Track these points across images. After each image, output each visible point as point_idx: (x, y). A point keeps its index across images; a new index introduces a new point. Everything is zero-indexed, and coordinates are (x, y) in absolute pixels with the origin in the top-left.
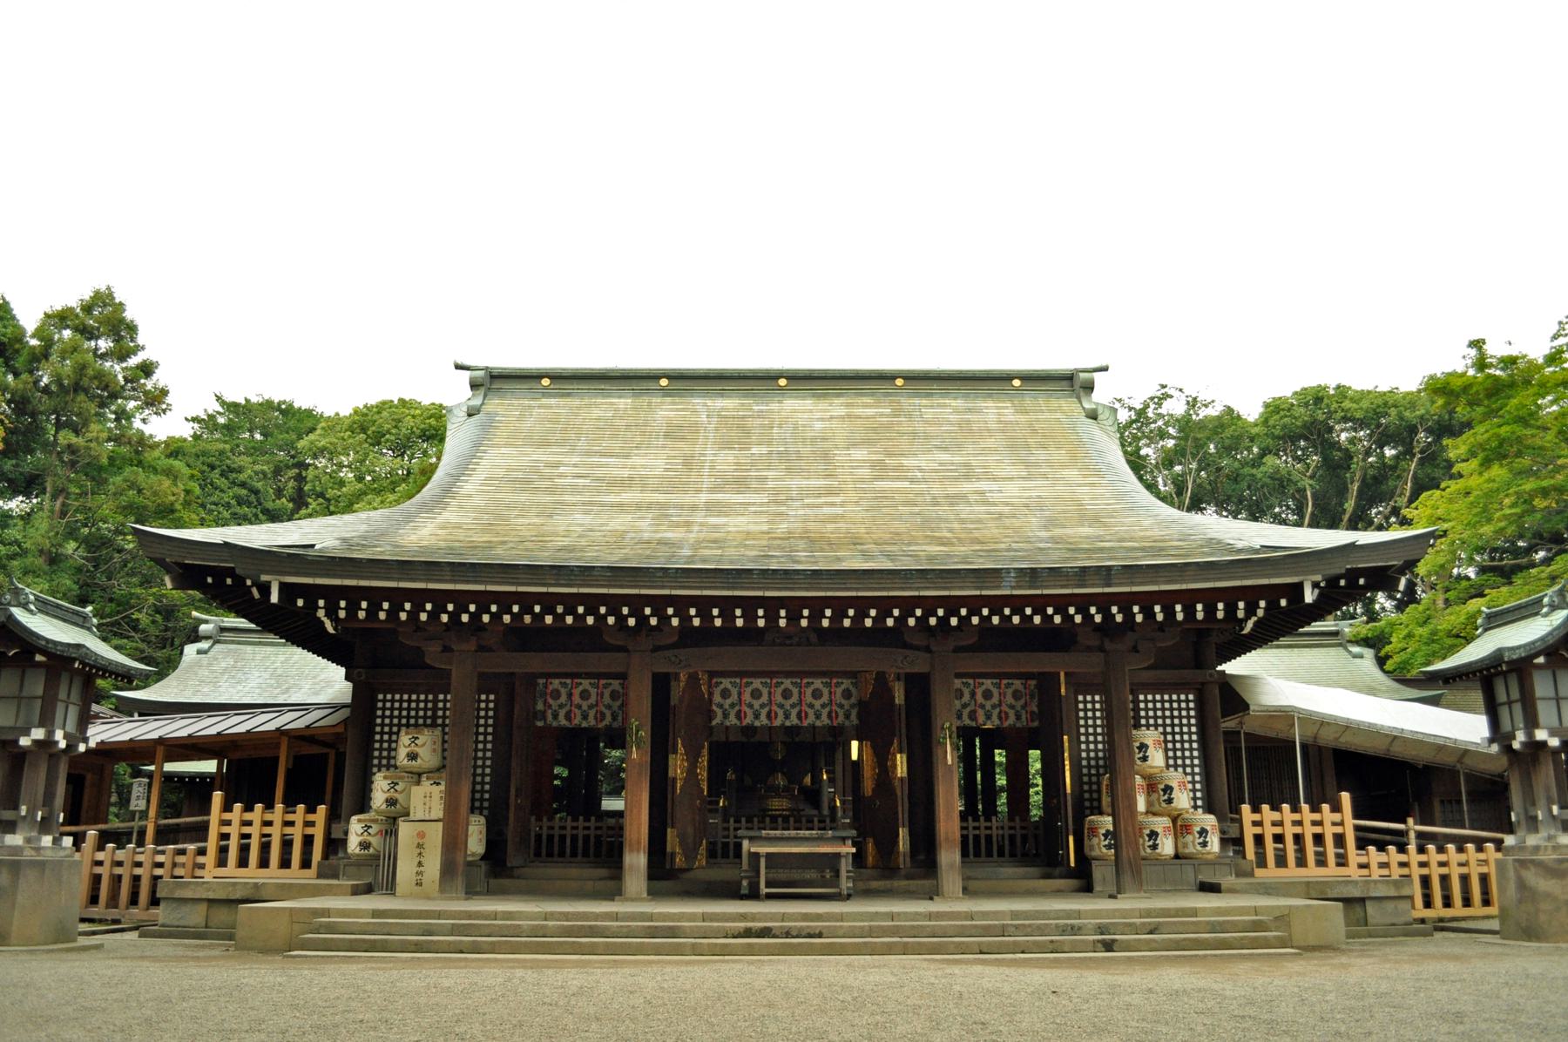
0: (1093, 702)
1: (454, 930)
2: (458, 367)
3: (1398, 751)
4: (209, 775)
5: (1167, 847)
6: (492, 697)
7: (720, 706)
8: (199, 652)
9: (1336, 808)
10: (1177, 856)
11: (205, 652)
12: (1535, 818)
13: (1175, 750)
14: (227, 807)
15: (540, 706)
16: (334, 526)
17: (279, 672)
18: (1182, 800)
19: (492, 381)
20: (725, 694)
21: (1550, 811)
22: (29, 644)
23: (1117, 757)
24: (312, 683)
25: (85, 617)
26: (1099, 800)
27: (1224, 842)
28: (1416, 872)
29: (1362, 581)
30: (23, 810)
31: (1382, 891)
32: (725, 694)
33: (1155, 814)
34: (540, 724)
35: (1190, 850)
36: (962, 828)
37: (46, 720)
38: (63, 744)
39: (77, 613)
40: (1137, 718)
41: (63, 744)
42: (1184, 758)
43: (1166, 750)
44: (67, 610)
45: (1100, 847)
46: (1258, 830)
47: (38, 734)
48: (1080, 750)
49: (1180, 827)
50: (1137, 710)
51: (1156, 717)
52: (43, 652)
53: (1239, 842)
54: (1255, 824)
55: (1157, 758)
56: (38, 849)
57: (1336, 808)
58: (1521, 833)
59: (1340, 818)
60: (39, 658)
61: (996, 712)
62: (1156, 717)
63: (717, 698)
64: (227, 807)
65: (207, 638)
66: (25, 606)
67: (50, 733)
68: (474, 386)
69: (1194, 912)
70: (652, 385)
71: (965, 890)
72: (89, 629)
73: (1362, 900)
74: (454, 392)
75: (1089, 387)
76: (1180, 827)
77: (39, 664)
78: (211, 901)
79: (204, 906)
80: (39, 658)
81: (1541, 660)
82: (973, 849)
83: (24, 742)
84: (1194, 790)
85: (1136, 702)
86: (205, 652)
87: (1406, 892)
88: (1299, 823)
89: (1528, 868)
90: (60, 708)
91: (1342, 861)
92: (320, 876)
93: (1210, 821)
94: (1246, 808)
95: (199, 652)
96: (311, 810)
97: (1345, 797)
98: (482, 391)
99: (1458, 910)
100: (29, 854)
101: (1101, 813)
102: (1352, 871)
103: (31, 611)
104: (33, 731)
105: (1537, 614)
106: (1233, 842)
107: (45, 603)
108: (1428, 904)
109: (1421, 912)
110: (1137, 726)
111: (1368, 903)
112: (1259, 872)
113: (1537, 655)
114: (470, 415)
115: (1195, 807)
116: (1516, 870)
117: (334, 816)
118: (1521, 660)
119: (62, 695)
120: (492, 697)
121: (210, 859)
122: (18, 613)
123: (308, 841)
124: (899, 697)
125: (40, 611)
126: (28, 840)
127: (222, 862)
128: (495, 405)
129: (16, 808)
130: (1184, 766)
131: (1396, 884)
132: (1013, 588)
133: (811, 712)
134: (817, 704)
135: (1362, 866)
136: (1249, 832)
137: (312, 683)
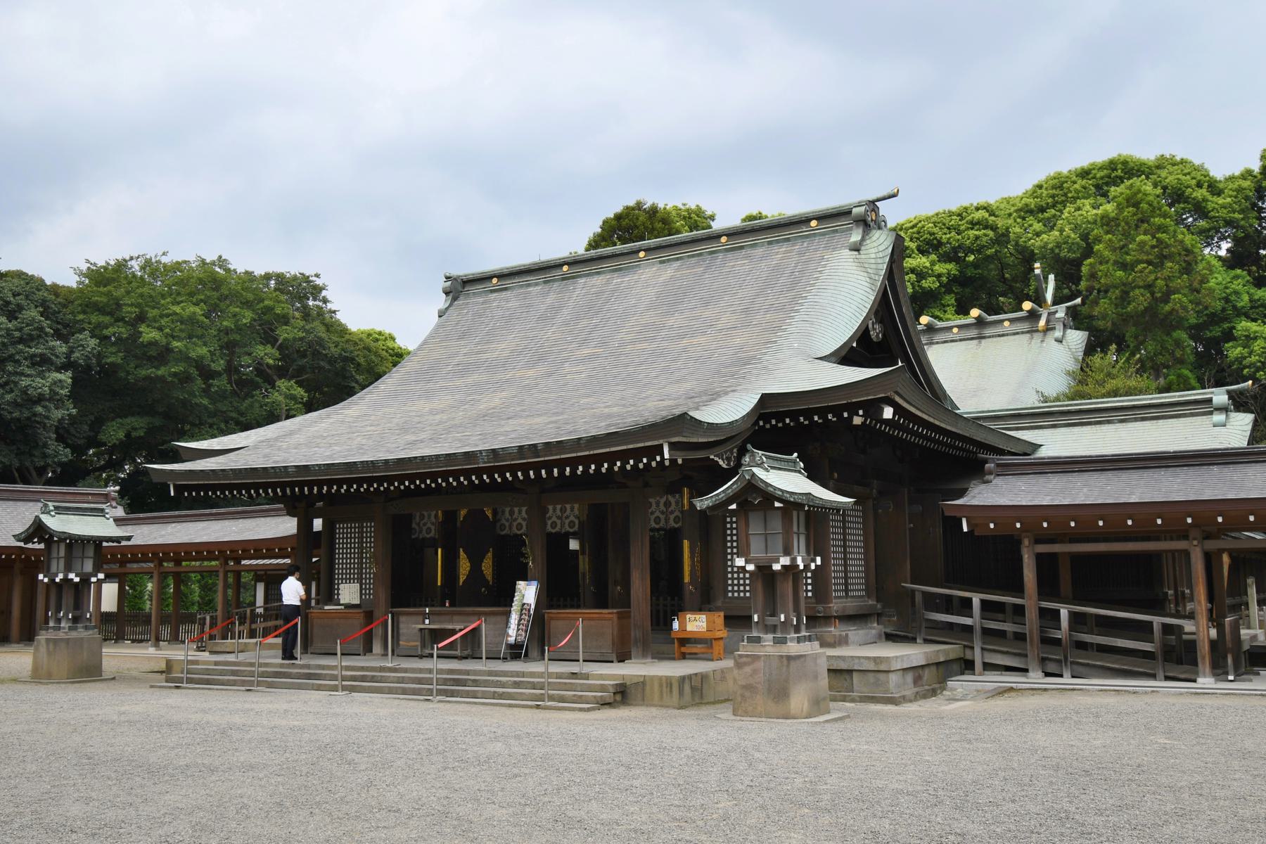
37: (787, 551)
39: (788, 461)
47: (785, 561)
60: (777, 504)
67: (794, 560)
70: (557, 273)
73: (850, 672)
80: (777, 504)
81: (734, 507)
83: (777, 567)
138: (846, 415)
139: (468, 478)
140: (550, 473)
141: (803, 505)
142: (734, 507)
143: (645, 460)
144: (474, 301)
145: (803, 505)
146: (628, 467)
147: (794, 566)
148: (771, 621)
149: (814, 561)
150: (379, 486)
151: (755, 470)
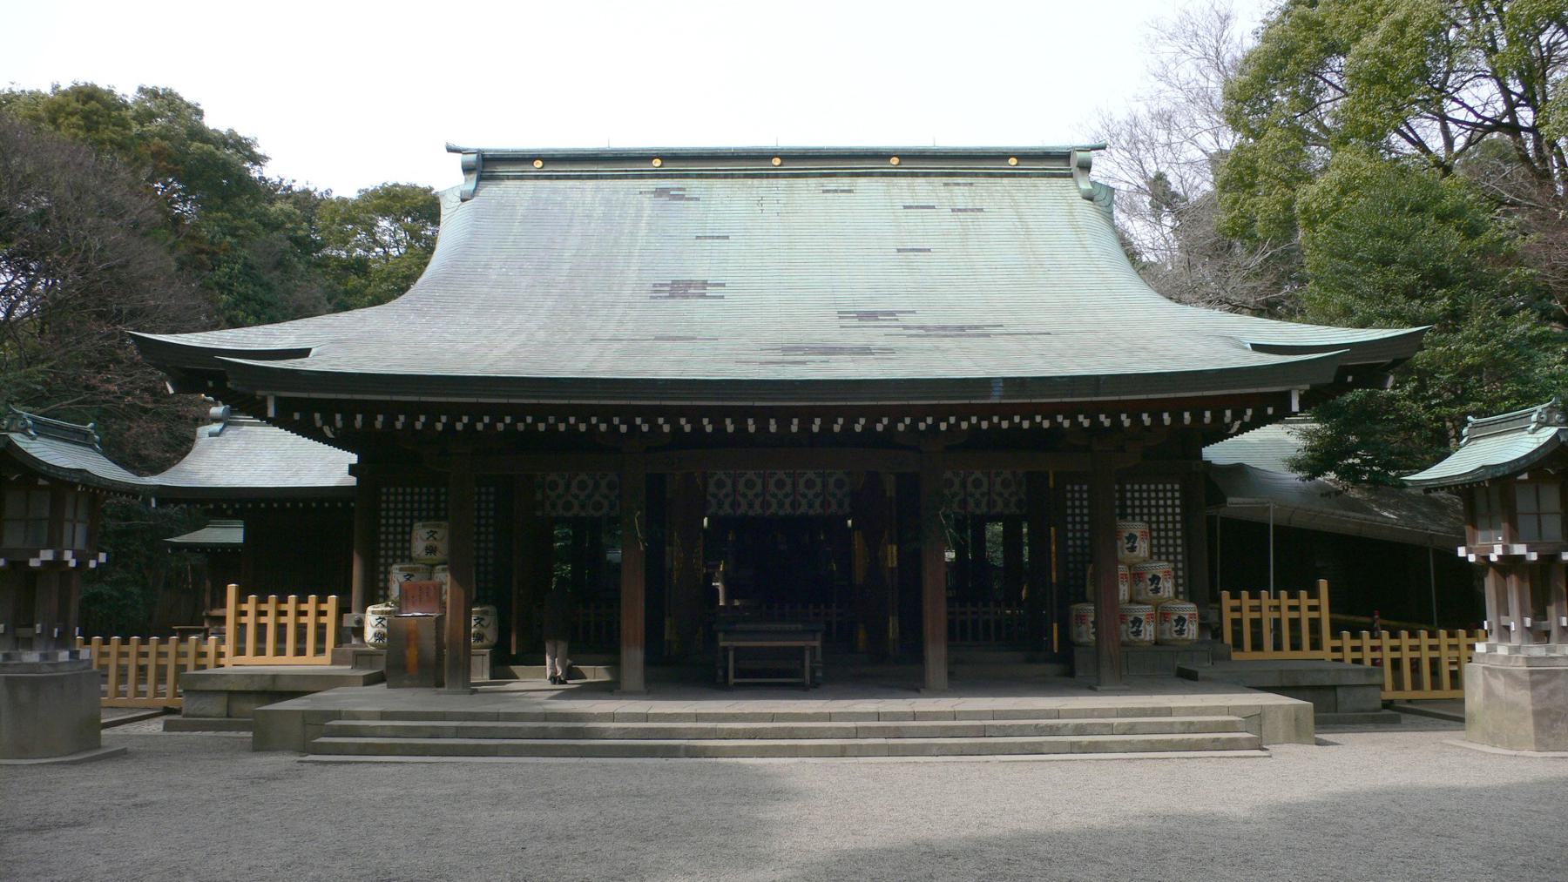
0: (1081, 491)
1: (459, 733)
2: (450, 150)
3: (1371, 727)
4: (234, 546)
5: (1148, 632)
6: (492, 489)
7: (714, 496)
8: (211, 435)
9: (1314, 594)
10: (1156, 643)
11: (217, 435)
12: (1508, 628)
13: (1159, 538)
14: (242, 598)
15: (539, 496)
16: (330, 325)
17: (290, 453)
18: (1167, 588)
19: (486, 167)
20: (720, 484)
21: (1523, 622)
22: (32, 470)
23: (1103, 537)
24: (323, 466)
25: (87, 435)
26: (1084, 586)
27: (1203, 627)
28: (1388, 656)
29: (1350, 379)
30: (38, 628)
31: (1353, 679)
32: (720, 484)
33: (1139, 603)
34: (539, 513)
35: (1167, 636)
36: (949, 613)
37: (55, 543)
38: (72, 563)
39: (78, 431)
40: (1123, 506)
41: (72, 563)
42: (1167, 545)
43: (1152, 538)
44: (68, 429)
45: (1086, 634)
46: (1236, 615)
47: (47, 555)
48: (1067, 539)
49: (1162, 616)
50: (1123, 499)
51: (1141, 507)
52: (44, 477)
53: (1218, 634)
54: (1234, 610)
55: (1143, 548)
56: (56, 665)
57: (1314, 594)
58: (1492, 640)
59: (1316, 604)
60: (41, 482)
61: (985, 500)
62: (1141, 507)
63: (712, 489)
64: (242, 598)
65: (216, 420)
66: (24, 431)
67: (59, 555)
68: (467, 169)
69: (1169, 712)
70: (644, 166)
71: (951, 674)
72: (92, 446)
73: (1334, 688)
74: (446, 178)
75: (1086, 167)
76: (1162, 616)
77: (42, 488)
78: (231, 693)
79: (223, 700)
80: (41, 482)
81: (1525, 476)
82: (957, 634)
83: (34, 563)
84: (1176, 577)
85: (1123, 491)
86: (217, 435)
87: (1376, 680)
88: (1278, 608)
89: (1496, 677)
90: (67, 527)
91: (1316, 645)
92: (334, 663)
93: (1188, 609)
94: (1225, 594)
95: (211, 435)
96: (322, 600)
97: (1323, 584)
98: (474, 176)
99: (1427, 692)
100: (47, 672)
101: (1085, 600)
102: (1326, 654)
103: (33, 438)
104: (42, 552)
105: (1524, 429)
106: (1211, 628)
107: (44, 424)
108: (1398, 686)
109: (1389, 694)
110: (1123, 516)
111: (1339, 691)
112: (1236, 656)
113: (1521, 473)
114: (463, 200)
115: (1177, 594)
116: (1485, 679)
117: (343, 609)
118: (1504, 477)
119: (69, 514)
120: (492, 489)
121: (228, 648)
122: (17, 438)
123: (321, 628)
124: (890, 491)
125: (39, 434)
126: (45, 657)
127: (240, 651)
128: (492, 190)
129: (32, 626)
130: (1167, 554)
131: (1368, 672)
132: (1003, 397)
133: (804, 502)
134: (810, 493)
135: (1335, 649)
136: (1228, 617)
137: (323, 466)
138: (1350, 379)
139: (1093, 417)
140: (1156, 418)
141: (76, 485)
142: (1525, 476)
143: (486, 419)
144: (510, 192)
145: (76, 485)
146: (459, 426)
147: (59, 562)
148: (23, 632)
149: (96, 557)
150: (535, 422)
151: (13, 436)
